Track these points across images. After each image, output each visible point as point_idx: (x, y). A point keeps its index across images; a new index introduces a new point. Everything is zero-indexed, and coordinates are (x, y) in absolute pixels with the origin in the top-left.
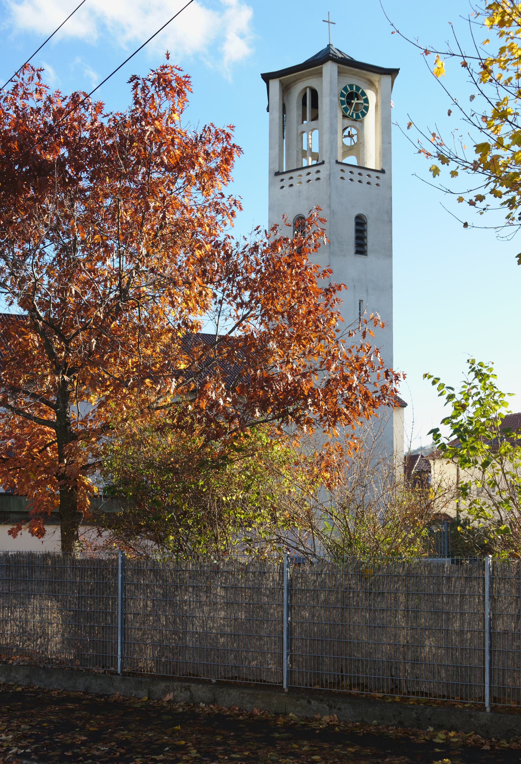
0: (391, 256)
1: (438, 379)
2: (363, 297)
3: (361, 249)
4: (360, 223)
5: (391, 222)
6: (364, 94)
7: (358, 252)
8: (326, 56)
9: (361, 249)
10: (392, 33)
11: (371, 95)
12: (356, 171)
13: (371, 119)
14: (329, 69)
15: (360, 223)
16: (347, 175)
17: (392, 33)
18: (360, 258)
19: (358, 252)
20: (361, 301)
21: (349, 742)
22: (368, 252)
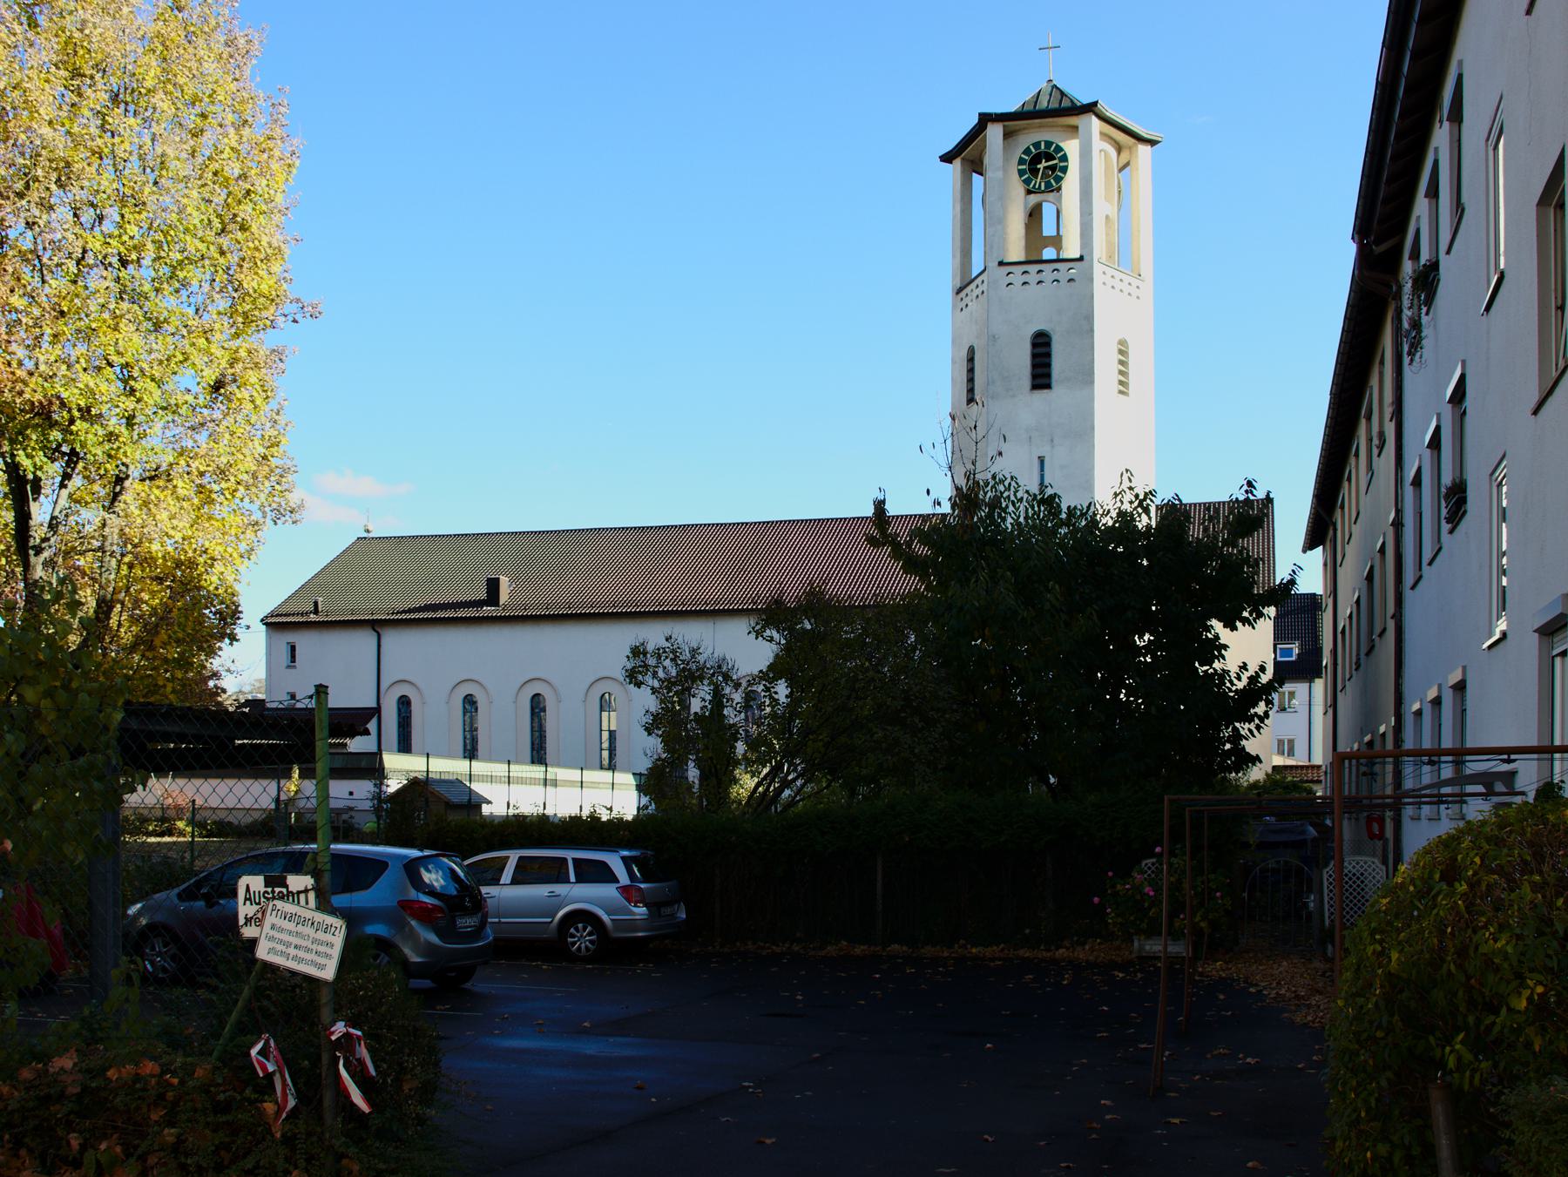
0: (1092, 382)
1: (1150, 494)
2: (1045, 451)
3: (1041, 377)
4: (1041, 345)
5: (1092, 330)
6: (1059, 149)
7: (1035, 387)
8: (985, 119)
9: (1041, 377)
10: (1250, 484)
11: (1071, 147)
12: (1033, 268)
13: (1071, 183)
14: (994, 132)
15: (1041, 345)
16: (1017, 278)
17: (1250, 484)
18: (1042, 395)
19: (1035, 387)
20: (1042, 460)
21: (1107, 1102)
22: (1054, 384)
